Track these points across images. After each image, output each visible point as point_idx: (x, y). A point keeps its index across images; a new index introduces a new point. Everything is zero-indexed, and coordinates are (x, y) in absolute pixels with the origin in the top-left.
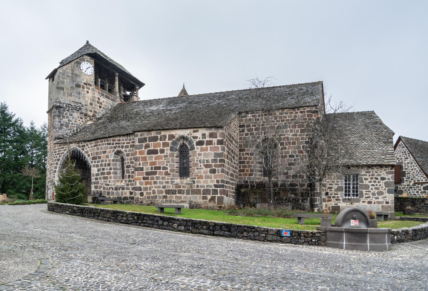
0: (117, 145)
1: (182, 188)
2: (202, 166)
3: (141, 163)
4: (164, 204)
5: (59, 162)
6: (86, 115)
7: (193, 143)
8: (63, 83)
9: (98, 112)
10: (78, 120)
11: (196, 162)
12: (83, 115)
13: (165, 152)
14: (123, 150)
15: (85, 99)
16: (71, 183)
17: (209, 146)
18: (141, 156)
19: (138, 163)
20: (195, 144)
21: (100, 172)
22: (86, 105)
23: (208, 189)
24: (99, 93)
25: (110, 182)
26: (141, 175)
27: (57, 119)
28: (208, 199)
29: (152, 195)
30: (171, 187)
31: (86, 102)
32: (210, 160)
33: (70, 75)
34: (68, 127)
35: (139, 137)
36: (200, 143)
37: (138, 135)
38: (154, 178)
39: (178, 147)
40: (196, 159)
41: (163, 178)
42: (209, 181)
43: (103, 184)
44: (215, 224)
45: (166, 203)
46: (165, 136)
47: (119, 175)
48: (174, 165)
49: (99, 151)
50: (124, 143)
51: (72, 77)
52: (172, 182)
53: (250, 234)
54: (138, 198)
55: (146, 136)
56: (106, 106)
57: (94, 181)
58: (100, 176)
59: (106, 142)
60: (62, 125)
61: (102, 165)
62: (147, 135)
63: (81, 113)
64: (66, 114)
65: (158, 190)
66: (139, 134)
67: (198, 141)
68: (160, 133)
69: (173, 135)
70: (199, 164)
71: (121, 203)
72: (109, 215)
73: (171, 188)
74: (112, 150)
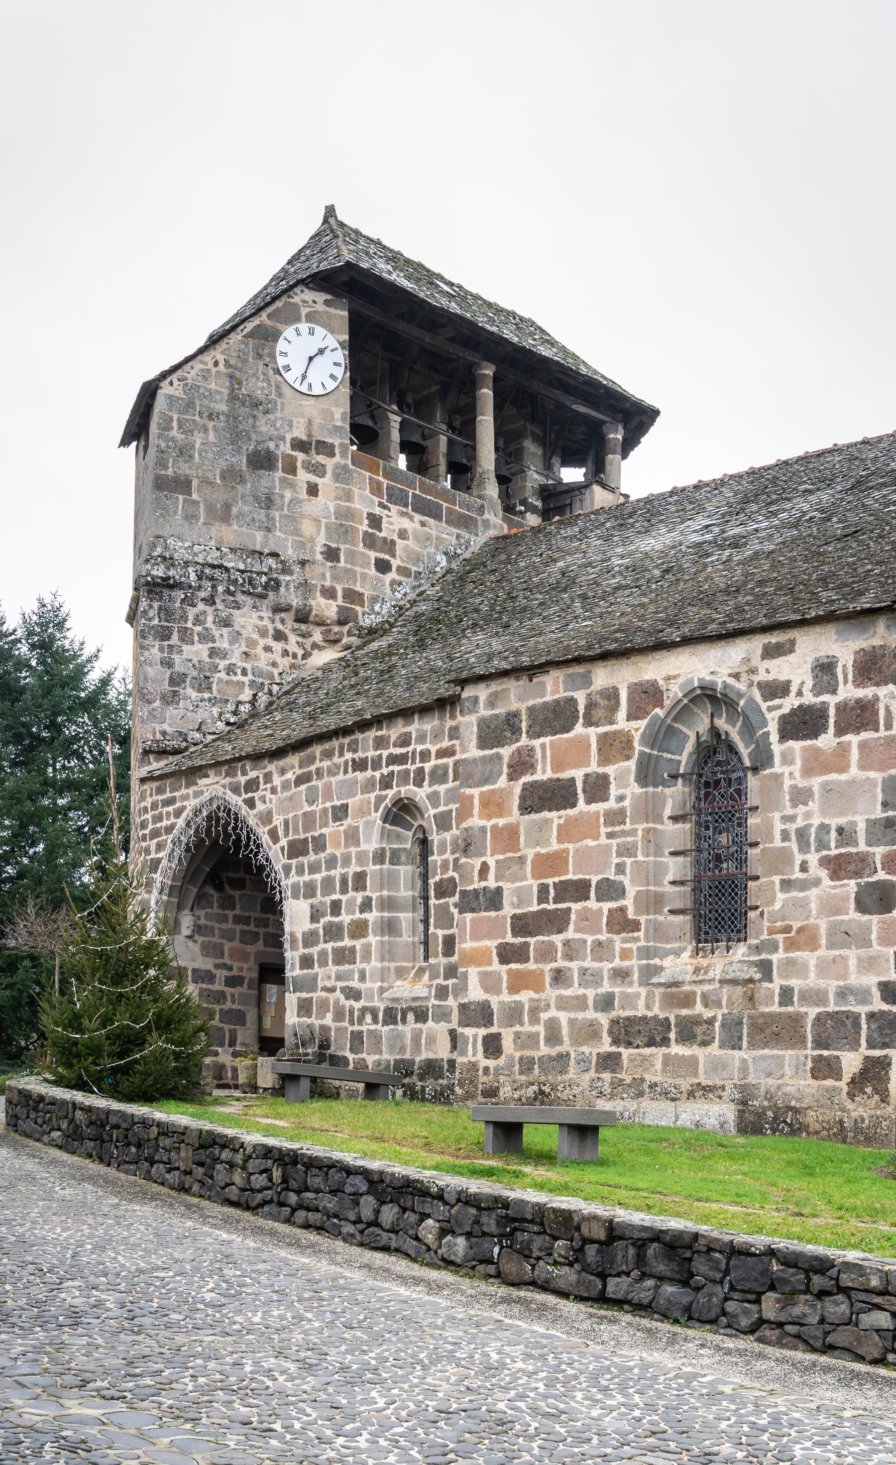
0: (396, 768)
1: (699, 1008)
2: (817, 871)
3: (491, 862)
4: (603, 1105)
5: (157, 877)
6: (303, 617)
7: (765, 723)
8: (185, 452)
9: (367, 593)
10: (259, 650)
11: (778, 843)
12: (289, 617)
13: (614, 791)
14: (421, 794)
15: (297, 532)
16: (115, 984)
17: (853, 739)
18: (488, 824)
19: (477, 863)
20: (773, 728)
21: (320, 926)
22: (303, 563)
23: (848, 1015)
24: (376, 489)
25: (362, 978)
26: (490, 937)
27: (155, 650)
28: (847, 1078)
29: (544, 1050)
30: (641, 1002)
31: (303, 545)
32: (861, 827)
33: (223, 407)
34: (209, 689)
35: (484, 712)
36: (803, 723)
37: (476, 700)
38: (552, 946)
39: (684, 758)
40: (778, 827)
41: (601, 950)
42: (852, 963)
43: (332, 990)
44: (614, 1233)
45: (612, 1097)
46: (612, 695)
47: (406, 938)
48: (660, 869)
49: (317, 807)
50: (425, 756)
51: (232, 416)
52: (649, 972)
53: (797, 1311)
54: (473, 1066)
55: (514, 706)
56: (418, 559)
57: (297, 972)
58: (322, 946)
59: (348, 756)
60: (177, 680)
61: (328, 883)
62: (520, 699)
63: (277, 609)
64: (198, 621)
65: (572, 1022)
66: (482, 692)
67: (794, 712)
68: (587, 681)
69: (654, 684)
70: (798, 858)
71: (412, 1095)
72: (184, 1157)
73: (641, 1011)
74: (372, 796)
